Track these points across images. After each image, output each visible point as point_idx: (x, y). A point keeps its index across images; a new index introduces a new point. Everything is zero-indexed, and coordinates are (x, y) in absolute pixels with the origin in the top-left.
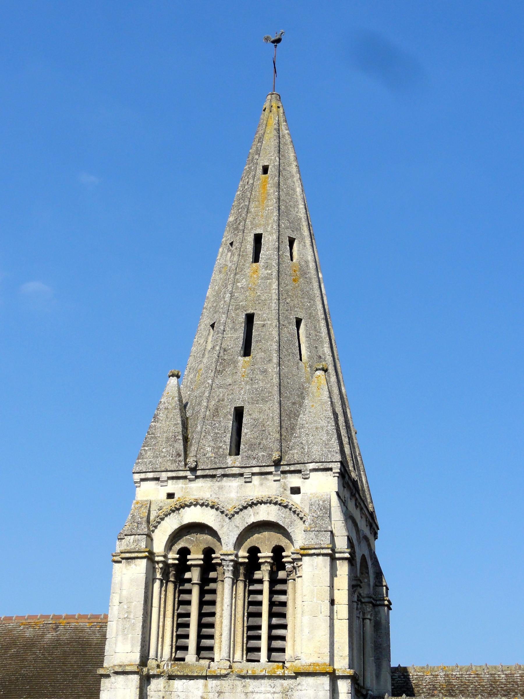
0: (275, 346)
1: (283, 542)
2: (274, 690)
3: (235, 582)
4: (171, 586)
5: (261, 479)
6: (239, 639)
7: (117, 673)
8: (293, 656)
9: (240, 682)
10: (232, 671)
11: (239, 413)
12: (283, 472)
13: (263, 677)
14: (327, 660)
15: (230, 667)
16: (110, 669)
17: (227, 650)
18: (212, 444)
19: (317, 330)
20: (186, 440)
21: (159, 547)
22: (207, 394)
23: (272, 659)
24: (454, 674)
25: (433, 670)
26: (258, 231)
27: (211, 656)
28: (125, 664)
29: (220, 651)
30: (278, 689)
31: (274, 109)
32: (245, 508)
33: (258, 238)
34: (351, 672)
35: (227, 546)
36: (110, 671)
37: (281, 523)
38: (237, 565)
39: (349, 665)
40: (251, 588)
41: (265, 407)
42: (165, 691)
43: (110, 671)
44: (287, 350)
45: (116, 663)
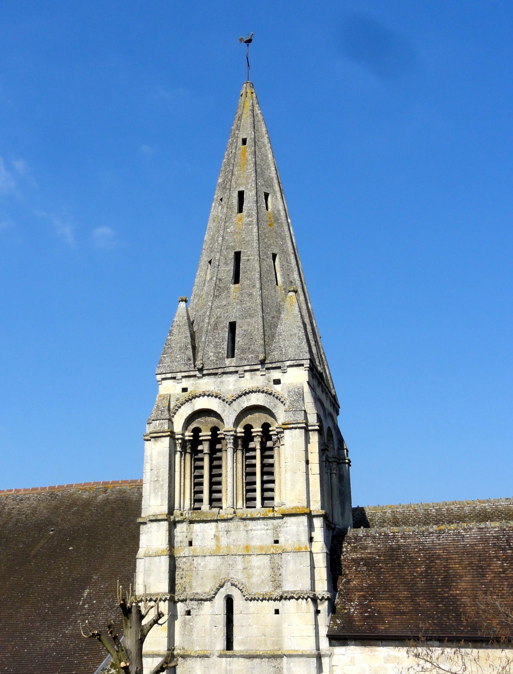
0: (257, 275)
1: (270, 420)
2: (267, 527)
3: (235, 451)
4: (188, 456)
5: (251, 375)
6: (240, 492)
7: (151, 521)
11: (233, 326)
12: (268, 369)
13: (259, 519)
14: (305, 504)
15: (235, 513)
17: (232, 501)
18: (214, 350)
19: (288, 261)
20: (194, 348)
21: (178, 428)
22: (208, 313)
25: (383, 508)
26: (241, 189)
27: (220, 505)
30: (270, 527)
31: (249, 94)
33: (241, 194)
34: (323, 512)
35: (228, 424)
37: (267, 406)
38: (236, 438)
40: (247, 454)
44: (266, 278)
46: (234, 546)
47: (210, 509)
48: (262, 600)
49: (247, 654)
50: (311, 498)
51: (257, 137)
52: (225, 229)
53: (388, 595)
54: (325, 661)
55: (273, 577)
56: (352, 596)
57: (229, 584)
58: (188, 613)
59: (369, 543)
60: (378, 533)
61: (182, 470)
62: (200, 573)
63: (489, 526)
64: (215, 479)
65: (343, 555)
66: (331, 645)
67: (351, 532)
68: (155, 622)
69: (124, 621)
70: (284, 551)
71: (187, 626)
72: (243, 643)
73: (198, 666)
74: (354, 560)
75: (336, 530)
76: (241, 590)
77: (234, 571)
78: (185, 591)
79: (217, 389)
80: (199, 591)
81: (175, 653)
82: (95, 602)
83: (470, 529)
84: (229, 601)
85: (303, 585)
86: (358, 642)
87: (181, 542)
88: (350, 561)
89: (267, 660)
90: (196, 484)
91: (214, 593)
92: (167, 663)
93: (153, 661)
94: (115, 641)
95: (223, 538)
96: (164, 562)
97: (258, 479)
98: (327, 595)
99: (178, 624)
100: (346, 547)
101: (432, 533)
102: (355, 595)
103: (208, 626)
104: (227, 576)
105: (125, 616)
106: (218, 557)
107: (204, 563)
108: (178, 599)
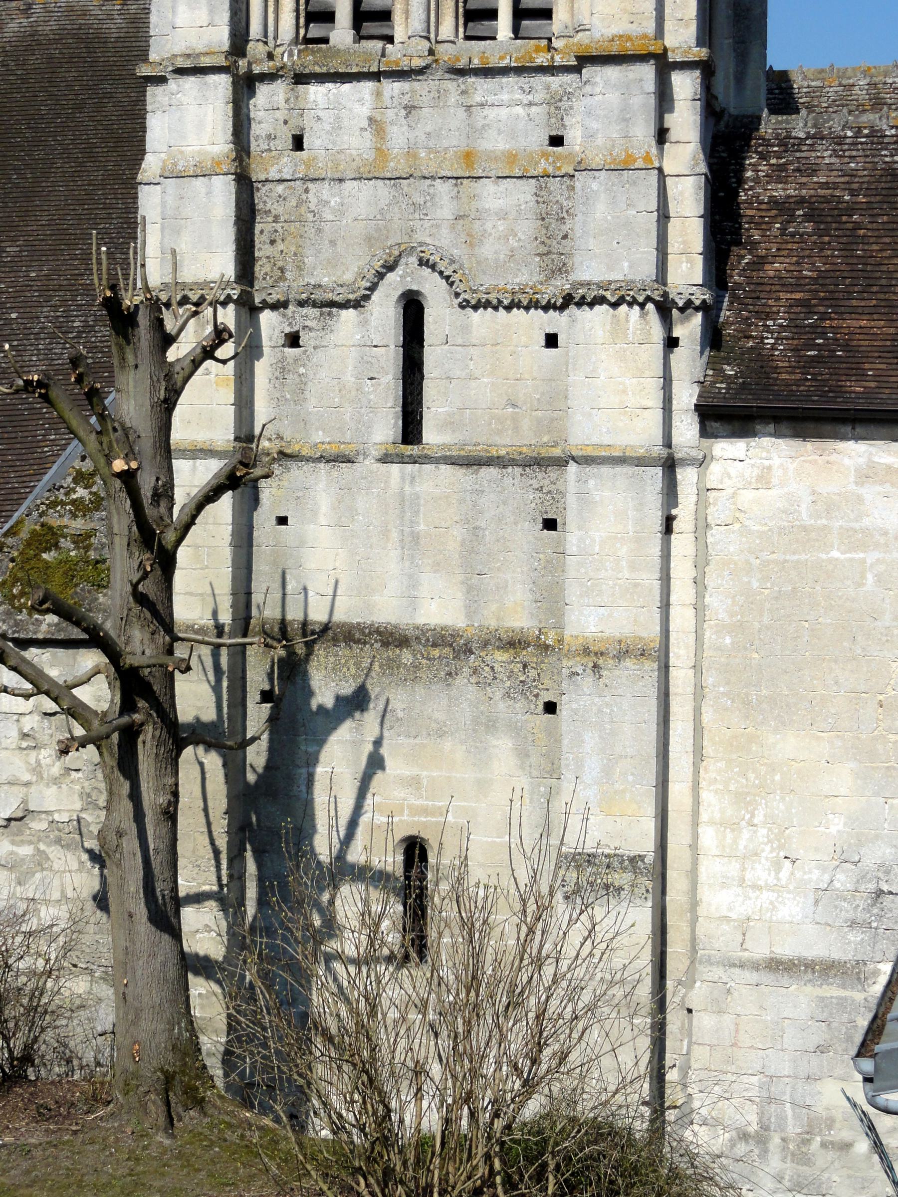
2: (530, 97)
7: (181, 72)
8: (570, 24)
9: (455, 83)
10: (436, 61)
13: (504, 71)
14: (650, 27)
15: (431, 52)
16: (164, 63)
17: (423, 17)
24: (890, 81)
25: (843, 74)
27: (386, 31)
28: (197, 51)
29: (407, 18)
30: (539, 96)
34: (702, 53)
36: (166, 67)
39: (698, 39)
42: (289, 110)
43: (166, 67)
45: (177, 50)
46: (429, 150)
48: (508, 308)
49: (463, 453)
50: (667, 11)
53: (874, 302)
54: (686, 477)
55: (543, 243)
56: (770, 302)
57: (413, 260)
58: (293, 340)
59: (825, 155)
60: (851, 128)
62: (327, 227)
65: (744, 190)
66: (705, 433)
67: (770, 125)
68: (208, 353)
69: (114, 349)
70: (582, 167)
71: (290, 376)
72: (448, 424)
73: (322, 485)
74: (776, 202)
75: (726, 118)
76: (447, 278)
77: (427, 224)
78: (282, 278)
82: (14, 316)
84: (413, 309)
85: (634, 265)
86: (784, 427)
87: (269, 137)
88: (764, 207)
89: (518, 470)
91: (368, 285)
92: (246, 465)
93: (194, 468)
94: (91, 404)
95: (395, 129)
96: (221, 194)
98: (701, 296)
99: (262, 369)
100: (754, 167)
102: (778, 299)
103: (349, 378)
104: (406, 239)
105: (117, 334)
106: (380, 183)
107: (337, 199)
108: (264, 301)
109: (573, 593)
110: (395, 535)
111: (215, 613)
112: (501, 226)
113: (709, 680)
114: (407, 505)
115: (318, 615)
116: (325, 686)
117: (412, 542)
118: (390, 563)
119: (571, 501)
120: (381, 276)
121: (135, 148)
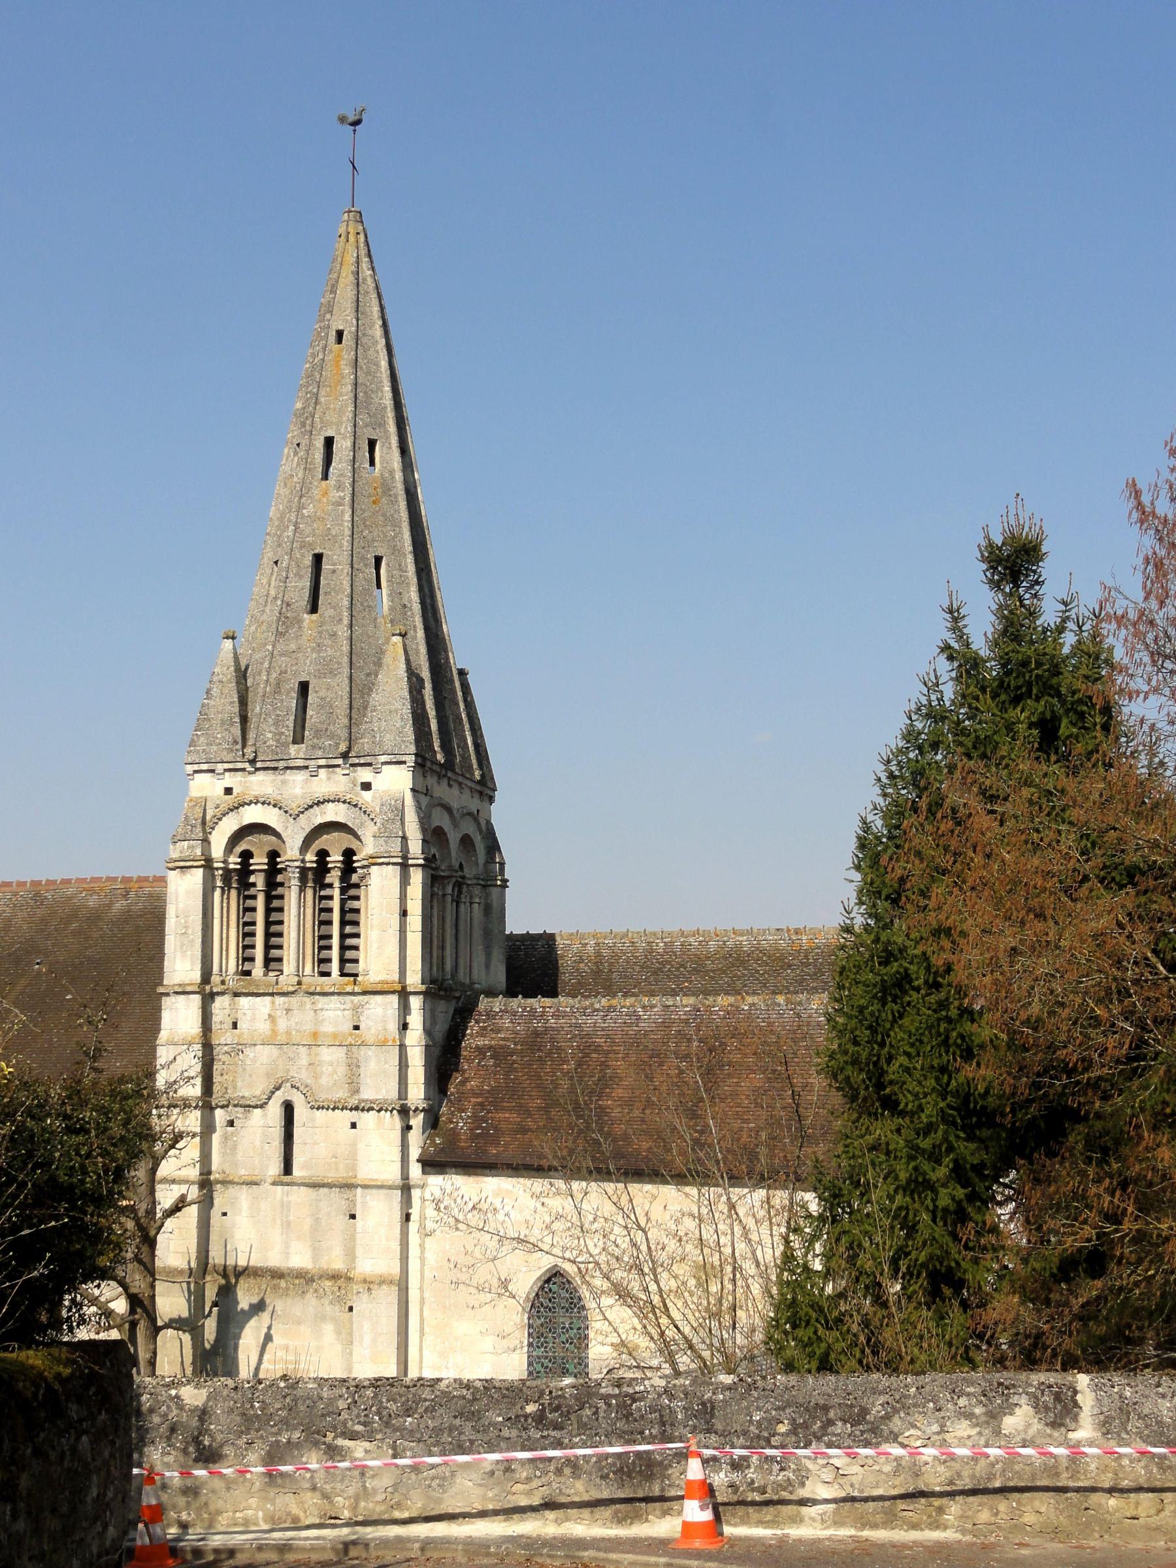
0: (346, 602)
1: (354, 845)
3: (302, 889)
4: (234, 893)
5: (328, 773)
6: (309, 951)
11: (304, 688)
12: (352, 765)
13: (332, 994)
14: (396, 977)
15: (299, 983)
18: (273, 729)
19: (402, 569)
20: (244, 719)
21: (217, 851)
22: (266, 665)
23: (345, 971)
25: (583, 937)
26: (330, 433)
30: (348, 1006)
31: (352, 238)
32: (311, 807)
33: (329, 442)
35: (291, 851)
37: (350, 824)
38: (303, 871)
40: (323, 893)
41: (333, 682)
44: (362, 604)
46: (298, 1031)
47: (266, 975)
48: (333, 1109)
51: (361, 328)
52: (300, 507)
54: (416, 1194)
57: (288, 1085)
58: (231, 1123)
61: (225, 915)
62: (248, 1068)
63: (679, 1003)
64: (274, 928)
66: (424, 1173)
72: (304, 1167)
73: (243, 1197)
78: (226, 1093)
79: (277, 792)
80: (246, 1094)
81: (212, 1178)
83: (652, 1007)
84: (288, 1108)
86: (459, 1170)
90: (245, 935)
97: (335, 930)
99: (216, 1138)
100: (473, 1028)
101: (597, 1010)
103: (258, 1143)
109: (359, 1252)
110: (279, 1222)
111: (189, 1262)
112: (330, 1069)
113: (426, 1295)
114: (285, 1207)
115: (242, 1262)
116: (244, 1301)
117: (287, 1225)
118: (276, 1236)
119: (359, 1206)
120: (273, 1093)
121: (156, 1028)
